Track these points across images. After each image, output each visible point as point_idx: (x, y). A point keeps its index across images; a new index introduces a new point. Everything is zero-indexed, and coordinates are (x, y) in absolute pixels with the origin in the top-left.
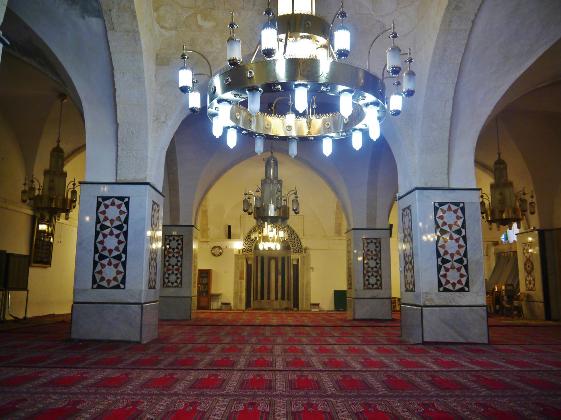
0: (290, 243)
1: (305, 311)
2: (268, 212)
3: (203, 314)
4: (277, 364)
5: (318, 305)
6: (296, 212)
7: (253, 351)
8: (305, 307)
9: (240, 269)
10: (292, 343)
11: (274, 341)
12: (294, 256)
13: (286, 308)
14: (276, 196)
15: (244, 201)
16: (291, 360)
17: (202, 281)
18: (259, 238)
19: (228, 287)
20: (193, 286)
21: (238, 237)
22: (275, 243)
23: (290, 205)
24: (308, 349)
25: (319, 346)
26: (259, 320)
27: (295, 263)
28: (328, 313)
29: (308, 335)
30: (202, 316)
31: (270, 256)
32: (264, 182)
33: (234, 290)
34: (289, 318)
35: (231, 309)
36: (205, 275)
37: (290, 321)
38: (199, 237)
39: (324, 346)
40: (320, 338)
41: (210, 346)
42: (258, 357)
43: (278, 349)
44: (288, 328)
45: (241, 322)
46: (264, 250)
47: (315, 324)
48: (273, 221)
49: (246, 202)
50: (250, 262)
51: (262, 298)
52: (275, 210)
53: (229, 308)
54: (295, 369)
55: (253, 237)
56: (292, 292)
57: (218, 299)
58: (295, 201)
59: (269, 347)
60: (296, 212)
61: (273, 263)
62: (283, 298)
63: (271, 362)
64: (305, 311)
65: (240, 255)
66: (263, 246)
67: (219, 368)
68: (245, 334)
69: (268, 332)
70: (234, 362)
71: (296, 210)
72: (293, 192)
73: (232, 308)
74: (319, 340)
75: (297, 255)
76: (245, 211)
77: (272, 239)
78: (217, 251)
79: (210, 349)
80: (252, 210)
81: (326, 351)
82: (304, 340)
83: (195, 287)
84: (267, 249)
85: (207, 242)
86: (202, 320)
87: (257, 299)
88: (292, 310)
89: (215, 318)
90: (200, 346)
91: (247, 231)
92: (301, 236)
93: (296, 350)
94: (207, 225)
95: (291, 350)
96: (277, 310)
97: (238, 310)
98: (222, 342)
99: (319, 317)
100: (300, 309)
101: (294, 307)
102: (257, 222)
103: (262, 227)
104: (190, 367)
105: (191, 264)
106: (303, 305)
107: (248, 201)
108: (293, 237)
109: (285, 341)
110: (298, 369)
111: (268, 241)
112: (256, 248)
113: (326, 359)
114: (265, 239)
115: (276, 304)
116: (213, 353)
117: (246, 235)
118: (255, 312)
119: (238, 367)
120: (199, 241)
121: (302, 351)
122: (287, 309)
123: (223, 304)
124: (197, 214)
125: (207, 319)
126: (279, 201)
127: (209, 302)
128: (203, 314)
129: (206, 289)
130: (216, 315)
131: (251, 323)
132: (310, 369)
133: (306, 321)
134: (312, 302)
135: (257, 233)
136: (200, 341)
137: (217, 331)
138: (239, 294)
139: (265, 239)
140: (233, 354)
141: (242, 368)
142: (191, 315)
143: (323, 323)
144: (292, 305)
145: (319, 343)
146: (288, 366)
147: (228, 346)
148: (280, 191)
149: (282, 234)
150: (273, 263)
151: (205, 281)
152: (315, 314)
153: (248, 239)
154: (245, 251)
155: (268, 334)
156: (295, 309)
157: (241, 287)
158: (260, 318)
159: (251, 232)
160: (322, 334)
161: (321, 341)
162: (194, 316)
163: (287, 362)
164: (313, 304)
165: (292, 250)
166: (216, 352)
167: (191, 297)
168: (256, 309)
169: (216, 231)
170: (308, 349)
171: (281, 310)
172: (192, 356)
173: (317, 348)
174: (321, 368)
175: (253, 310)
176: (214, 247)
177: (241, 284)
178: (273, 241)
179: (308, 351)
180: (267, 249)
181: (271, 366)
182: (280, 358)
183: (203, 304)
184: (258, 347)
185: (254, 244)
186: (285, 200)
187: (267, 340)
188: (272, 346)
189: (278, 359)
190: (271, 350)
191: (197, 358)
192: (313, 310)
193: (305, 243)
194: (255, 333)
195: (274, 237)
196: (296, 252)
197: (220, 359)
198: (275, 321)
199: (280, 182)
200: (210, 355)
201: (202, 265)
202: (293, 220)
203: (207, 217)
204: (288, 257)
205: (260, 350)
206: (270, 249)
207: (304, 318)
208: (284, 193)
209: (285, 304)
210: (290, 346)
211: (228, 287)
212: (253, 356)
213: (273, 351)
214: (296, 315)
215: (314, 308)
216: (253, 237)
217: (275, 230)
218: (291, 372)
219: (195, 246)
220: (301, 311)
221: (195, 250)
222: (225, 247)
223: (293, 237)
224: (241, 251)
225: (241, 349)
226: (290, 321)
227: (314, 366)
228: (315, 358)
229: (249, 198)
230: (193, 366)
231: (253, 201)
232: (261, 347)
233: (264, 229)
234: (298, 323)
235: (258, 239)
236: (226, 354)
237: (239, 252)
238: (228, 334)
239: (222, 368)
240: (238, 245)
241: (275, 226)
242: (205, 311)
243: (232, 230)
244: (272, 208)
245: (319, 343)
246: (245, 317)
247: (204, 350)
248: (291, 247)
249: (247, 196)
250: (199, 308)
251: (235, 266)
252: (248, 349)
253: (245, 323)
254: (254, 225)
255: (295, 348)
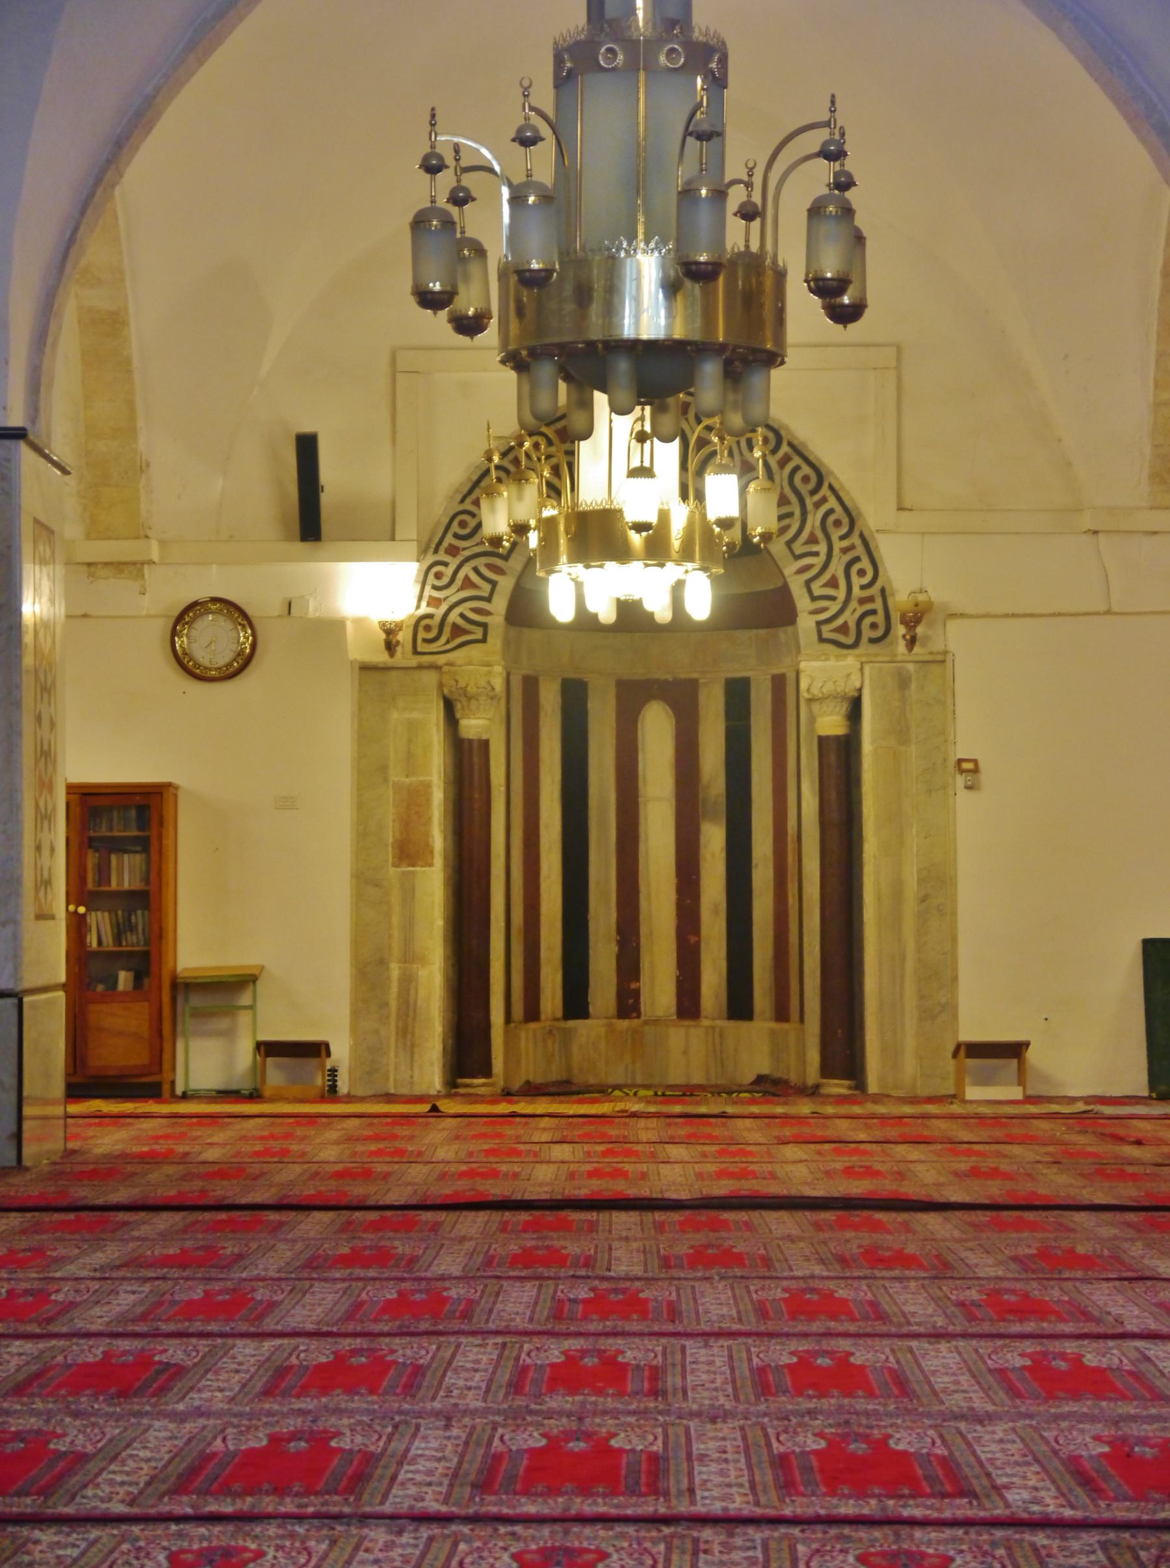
0: (790, 568)
1: (914, 1100)
2: (611, 310)
3: (116, 1133)
4: (702, 1472)
5: (1015, 1050)
6: (840, 302)
7: (516, 1386)
8: (910, 1067)
9: (396, 776)
10: (816, 1327)
11: (673, 1312)
12: (823, 673)
13: (760, 1079)
14: (681, 175)
15: (419, 223)
16: (816, 1444)
17: (103, 873)
18: (548, 527)
19: (306, 921)
20: (28, 908)
21: (375, 532)
22: (672, 572)
23: (792, 256)
24: (942, 1364)
25: (1030, 1347)
26: (552, 1164)
27: (832, 723)
28: (1094, 1116)
29: (942, 1269)
30: (108, 1142)
31: (640, 659)
32: (574, 65)
33: (357, 943)
34: (792, 1152)
35: (331, 1093)
36: (124, 824)
37: (802, 1171)
38: (71, 530)
39: (1070, 1347)
40: (1035, 1290)
41: (173, 1352)
42: (556, 1426)
43: (707, 1371)
44: (779, 1223)
45: (410, 1181)
46: (586, 622)
47: (994, 1190)
48: (657, 377)
49: (437, 230)
50: (473, 725)
51: (576, 1003)
52: (671, 288)
53: (320, 1081)
54: (848, 1508)
55: (497, 520)
56: (809, 960)
57: (231, 1011)
58: (834, 211)
59: (632, 1353)
60: (840, 302)
61: (657, 729)
62: (739, 1005)
63: (656, 1464)
64: (914, 1100)
65: (400, 661)
66: (578, 591)
67: (246, 1504)
68: (449, 1263)
69: (625, 1248)
70: (368, 1459)
71: (842, 284)
72: (814, 140)
73: (343, 1087)
74: (1028, 1308)
75: (850, 661)
76: (428, 300)
77: (646, 523)
78: (213, 641)
79: (177, 1371)
80: (483, 291)
81: (1097, 1383)
82: (913, 1302)
83: (43, 916)
84: (606, 613)
85: (131, 568)
86: (109, 1169)
87: (532, 1013)
88: (813, 1092)
89: (212, 1154)
90: (93, 1352)
91: (452, 474)
92: (875, 514)
93: (847, 1378)
94: (130, 431)
95: (807, 1377)
96: (689, 1092)
97: (389, 1098)
98: (270, 1324)
99: (1027, 1140)
100: (873, 1087)
101: (827, 1070)
102: (528, 397)
103: (561, 437)
104: (28, 1504)
105: (13, 732)
106: (895, 1049)
107: (448, 223)
108: (814, 519)
109: (762, 1311)
110: (871, 1507)
111: (623, 554)
112: (525, 610)
113: (1088, 1443)
114: (598, 536)
115: (685, 1052)
116: (196, 1399)
117: (441, 508)
118: (522, 1107)
119: (399, 1499)
120: (68, 563)
121: (900, 1384)
122: (770, 1086)
123: (268, 1049)
124: (41, 339)
125: (151, 1159)
126: (704, 218)
127: (159, 1044)
128: (116, 1133)
129: (133, 942)
130: (220, 1136)
131: (496, 1190)
132: (962, 1508)
133: (926, 1172)
134: (968, 1034)
135: (532, 490)
136: (97, 1317)
137: (230, 1248)
138: (395, 970)
139: (598, 536)
140: (358, 1403)
141: (433, 1505)
142: (18, 1136)
143: (1057, 1183)
144: (814, 1056)
145: (1030, 1327)
146: (788, 1487)
147: (320, 1353)
148: (710, 135)
149: (723, 494)
150: (657, 729)
151: (126, 873)
152: (991, 1120)
153: (455, 542)
154: (432, 635)
155: (626, 1262)
156: (838, 1087)
157: (409, 925)
158: (561, 1152)
159: (478, 487)
160: (1055, 1262)
161: (1040, 1310)
162: (40, 1148)
163: (783, 1462)
164: (977, 1050)
165: (806, 623)
166: (223, 1394)
167: (17, 997)
168: (532, 1090)
169: (204, 493)
170: (942, 1364)
171: (728, 1091)
172: (33, 1423)
173: (1014, 1358)
174: (1052, 1506)
175: (507, 1094)
176: (190, 612)
177: (409, 893)
178: (657, 549)
179: (941, 1381)
180: (606, 613)
181: (654, 1489)
182: (725, 1429)
183: (117, 1051)
184: (554, 1352)
185: (506, 584)
186: (748, 213)
187: (620, 1304)
188: (658, 1345)
189: (711, 1441)
190: (655, 1374)
191: (74, 1436)
192: (973, 1093)
193: (906, 571)
194: (526, 1259)
195: (664, 516)
196: (842, 639)
197: (258, 1440)
198: (678, 1171)
199: (708, 59)
200: (181, 1418)
201: (96, 757)
202: (811, 382)
203: (125, 365)
204: (779, 683)
205: (567, 1376)
206: (631, 614)
207: (901, 1150)
208: (741, 153)
209: (754, 1048)
210: (803, 1346)
211: (306, 921)
212: (517, 1417)
213: (672, 1380)
214: (843, 1128)
215: (986, 1080)
216: (497, 520)
217: (667, 455)
218: (818, 1532)
219: (36, 604)
220: (878, 1099)
221: (43, 625)
222: (276, 609)
223: (814, 519)
224: (404, 636)
225: (418, 1371)
226: (798, 1170)
227: (998, 1489)
228: (1001, 1429)
229: (460, 198)
230: (46, 1491)
231: (494, 222)
232: (571, 1358)
233: (584, 448)
234: (858, 1188)
235: (533, 539)
236: (307, 1404)
237: (390, 646)
238: (315, 1265)
239: (268, 1504)
240: (376, 590)
241: (668, 421)
242: (128, 1107)
243: (326, 474)
244: (646, 268)
245: (1030, 1327)
246: (442, 1152)
247: (128, 1380)
248: (803, 603)
249: (446, 180)
250: (81, 1085)
251: (360, 757)
252: (470, 1369)
253: (446, 1190)
254: (507, 423)
255: (843, 1361)
